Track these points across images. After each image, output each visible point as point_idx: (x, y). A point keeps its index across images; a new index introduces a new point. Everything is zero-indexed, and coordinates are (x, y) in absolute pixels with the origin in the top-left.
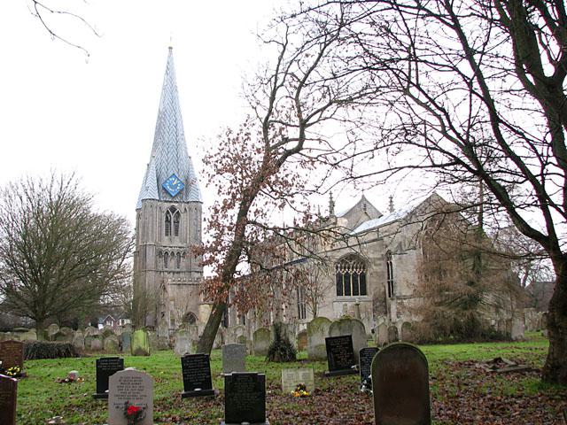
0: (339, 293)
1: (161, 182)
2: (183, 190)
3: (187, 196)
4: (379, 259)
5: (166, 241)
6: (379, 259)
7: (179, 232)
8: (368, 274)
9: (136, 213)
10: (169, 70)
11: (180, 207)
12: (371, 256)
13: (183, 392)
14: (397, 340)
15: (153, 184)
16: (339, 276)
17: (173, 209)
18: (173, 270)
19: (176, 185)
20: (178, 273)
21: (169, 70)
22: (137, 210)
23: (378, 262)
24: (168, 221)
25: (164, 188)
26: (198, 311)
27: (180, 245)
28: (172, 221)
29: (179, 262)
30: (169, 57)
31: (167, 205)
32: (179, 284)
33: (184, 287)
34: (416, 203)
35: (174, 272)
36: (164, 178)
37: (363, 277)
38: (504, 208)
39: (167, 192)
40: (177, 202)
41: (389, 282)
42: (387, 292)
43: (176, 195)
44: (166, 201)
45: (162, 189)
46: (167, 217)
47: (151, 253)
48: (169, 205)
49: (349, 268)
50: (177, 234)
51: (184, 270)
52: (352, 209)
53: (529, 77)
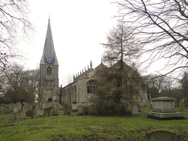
1: (46, 60)
2: (52, 62)
5: (47, 76)
10: (91, 63)
11: (52, 67)
16: (88, 87)
17: (49, 67)
18: (49, 85)
19: (50, 60)
20: (51, 86)
21: (91, 63)
24: (48, 71)
25: (46, 61)
26: (53, 98)
31: (47, 66)
35: (49, 86)
38: (177, 43)
39: (47, 62)
43: (50, 63)
45: (46, 61)
46: (48, 70)
49: (92, 84)
50: (51, 75)
51: (53, 85)
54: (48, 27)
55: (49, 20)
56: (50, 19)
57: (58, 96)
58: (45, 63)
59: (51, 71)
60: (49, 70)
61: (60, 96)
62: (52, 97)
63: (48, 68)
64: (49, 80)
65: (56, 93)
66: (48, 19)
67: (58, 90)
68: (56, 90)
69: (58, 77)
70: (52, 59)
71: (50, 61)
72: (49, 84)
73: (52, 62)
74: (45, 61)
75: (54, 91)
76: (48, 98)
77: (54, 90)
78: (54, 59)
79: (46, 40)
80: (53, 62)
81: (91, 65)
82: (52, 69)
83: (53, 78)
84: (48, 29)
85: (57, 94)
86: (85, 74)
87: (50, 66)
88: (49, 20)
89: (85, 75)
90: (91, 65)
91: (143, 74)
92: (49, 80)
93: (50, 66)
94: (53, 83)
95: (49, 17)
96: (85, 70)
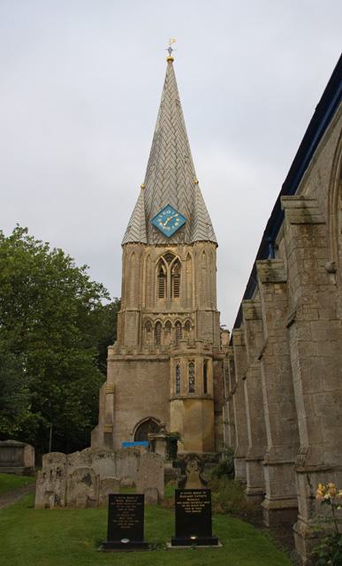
3: (191, 234)
7: (290, 321)
9: (121, 250)
10: (170, 85)
13: (106, 541)
15: (140, 221)
17: (169, 256)
21: (170, 85)
24: (162, 275)
25: (155, 227)
27: (182, 310)
28: (168, 276)
29: (178, 336)
30: (168, 69)
31: (160, 251)
32: (129, 360)
33: (139, 365)
34: (100, 402)
39: (159, 231)
40: (175, 245)
43: (173, 235)
44: (157, 245)
50: (176, 293)
53: (125, 541)
54: (165, 88)
57: (198, 404)
58: (147, 237)
59: (176, 278)
60: (167, 268)
61: (217, 405)
62: (166, 413)
63: (161, 262)
64: (168, 324)
66: (167, 55)
67: (199, 361)
68: (183, 362)
69: (213, 304)
74: (147, 225)
75: (173, 370)
77: (172, 363)
78: (192, 215)
79: (154, 141)
80: (187, 229)
82: (183, 264)
83: (188, 309)
84: (164, 96)
85: (192, 390)
87: (174, 249)
88: (170, 60)
92: (168, 324)
93: (174, 249)
95: (170, 50)
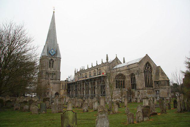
0: (117, 87)
4: (129, 76)
5: (49, 69)
6: (129, 76)
8: (125, 81)
12: (126, 75)
14: (86, 77)
15: (46, 51)
17: (52, 59)
20: (53, 79)
22: (147, 64)
23: (128, 77)
24: (50, 63)
25: (49, 53)
31: (50, 58)
36: (49, 50)
37: (124, 81)
39: (50, 54)
41: (132, 84)
42: (131, 87)
44: (50, 57)
45: (49, 53)
46: (50, 62)
47: (44, 74)
48: (50, 58)
52: (113, 61)
55: (54, 12)
56: (55, 11)
57: (66, 91)
65: (64, 87)
68: (64, 84)
70: (55, 51)
71: (53, 53)
72: (51, 77)
73: (54, 55)
75: (62, 85)
76: (54, 92)
81: (107, 59)
83: (55, 71)
86: (80, 73)
88: (54, 12)
89: (80, 75)
90: (107, 59)
91: (182, 83)
92: (51, 73)
94: (54, 76)
96: (88, 67)
